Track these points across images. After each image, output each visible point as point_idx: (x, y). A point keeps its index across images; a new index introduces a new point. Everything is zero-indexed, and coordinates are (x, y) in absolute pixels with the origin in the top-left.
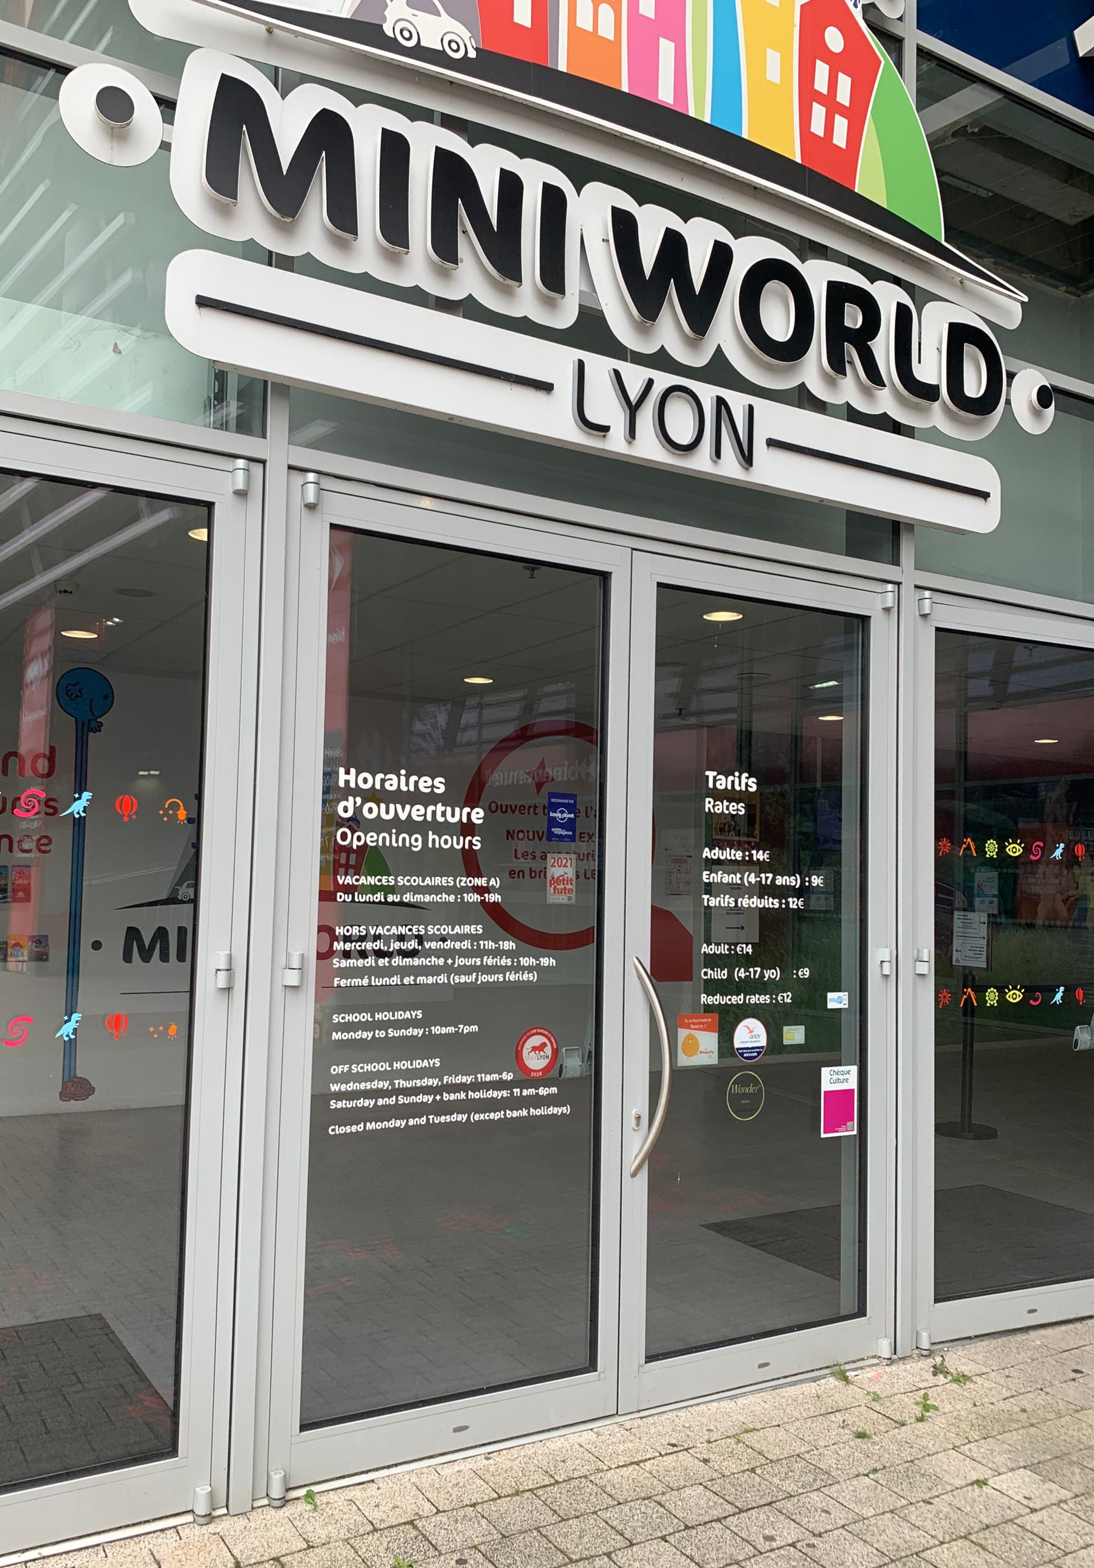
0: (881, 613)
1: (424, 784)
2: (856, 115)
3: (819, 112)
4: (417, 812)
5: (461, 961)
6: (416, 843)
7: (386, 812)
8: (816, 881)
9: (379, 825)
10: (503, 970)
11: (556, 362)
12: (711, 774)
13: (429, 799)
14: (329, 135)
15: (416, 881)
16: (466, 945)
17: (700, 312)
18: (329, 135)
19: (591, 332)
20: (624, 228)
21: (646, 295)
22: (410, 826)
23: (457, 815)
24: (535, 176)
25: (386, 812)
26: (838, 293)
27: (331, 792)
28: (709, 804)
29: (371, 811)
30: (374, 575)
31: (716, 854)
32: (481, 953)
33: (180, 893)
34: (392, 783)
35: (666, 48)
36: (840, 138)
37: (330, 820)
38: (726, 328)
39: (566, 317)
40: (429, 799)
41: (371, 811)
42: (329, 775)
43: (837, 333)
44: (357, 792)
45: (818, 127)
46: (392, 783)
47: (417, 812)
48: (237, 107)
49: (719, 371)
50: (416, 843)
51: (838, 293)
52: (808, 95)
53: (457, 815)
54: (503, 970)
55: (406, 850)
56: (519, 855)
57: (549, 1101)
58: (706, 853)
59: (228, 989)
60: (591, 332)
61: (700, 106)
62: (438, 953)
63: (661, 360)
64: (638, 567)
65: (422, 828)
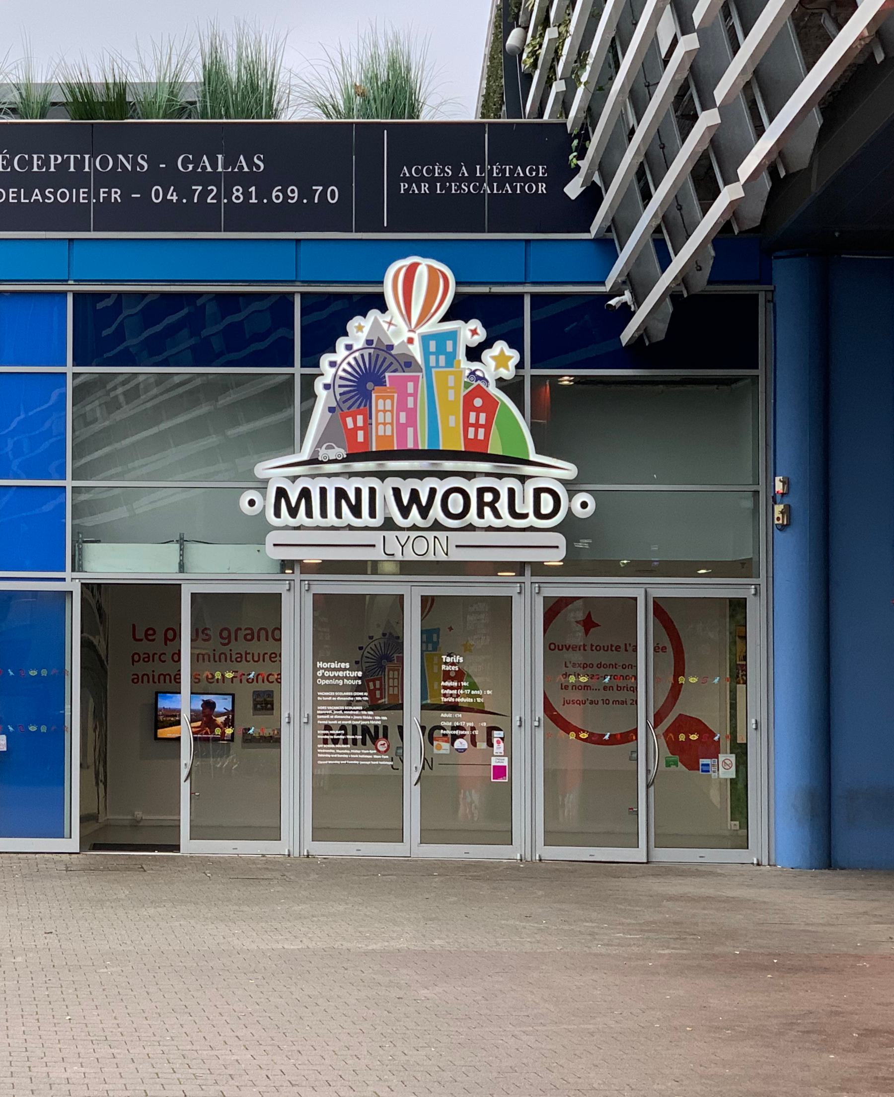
0: (517, 595)
1: (343, 665)
2: (488, 427)
3: (471, 431)
4: (341, 674)
5: (355, 717)
6: (341, 682)
7: (332, 674)
8: (489, 692)
9: (329, 678)
10: (369, 720)
11: (376, 537)
12: (444, 657)
13: (345, 669)
14: (305, 494)
15: (341, 694)
16: (357, 712)
17: (424, 512)
18: (305, 494)
19: (389, 525)
20: (397, 492)
21: (405, 512)
22: (338, 678)
23: (354, 674)
24: (365, 485)
25: (332, 674)
26: (481, 491)
27: (315, 669)
28: (443, 667)
29: (327, 674)
30: (324, 605)
31: (447, 684)
32: (362, 715)
33: (320, 454)
34: (333, 665)
35: (410, 431)
36: (481, 436)
37: (315, 677)
38: (436, 512)
39: (378, 521)
40: (345, 669)
41: (327, 674)
42: (315, 665)
43: (481, 504)
44: (323, 668)
45: (471, 435)
46: (333, 665)
47: (341, 674)
48: (281, 493)
49: (437, 526)
50: (341, 682)
51: (481, 491)
52: (466, 425)
53: (354, 674)
54: (369, 720)
55: (338, 685)
56: (140, 634)
57: (386, 760)
58: (443, 683)
59: (289, 723)
60: (389, 525)
61: (423, 442)
62: (349, 715)
63: (414, 528)
64: (413, 594)
65: (342, 678)
